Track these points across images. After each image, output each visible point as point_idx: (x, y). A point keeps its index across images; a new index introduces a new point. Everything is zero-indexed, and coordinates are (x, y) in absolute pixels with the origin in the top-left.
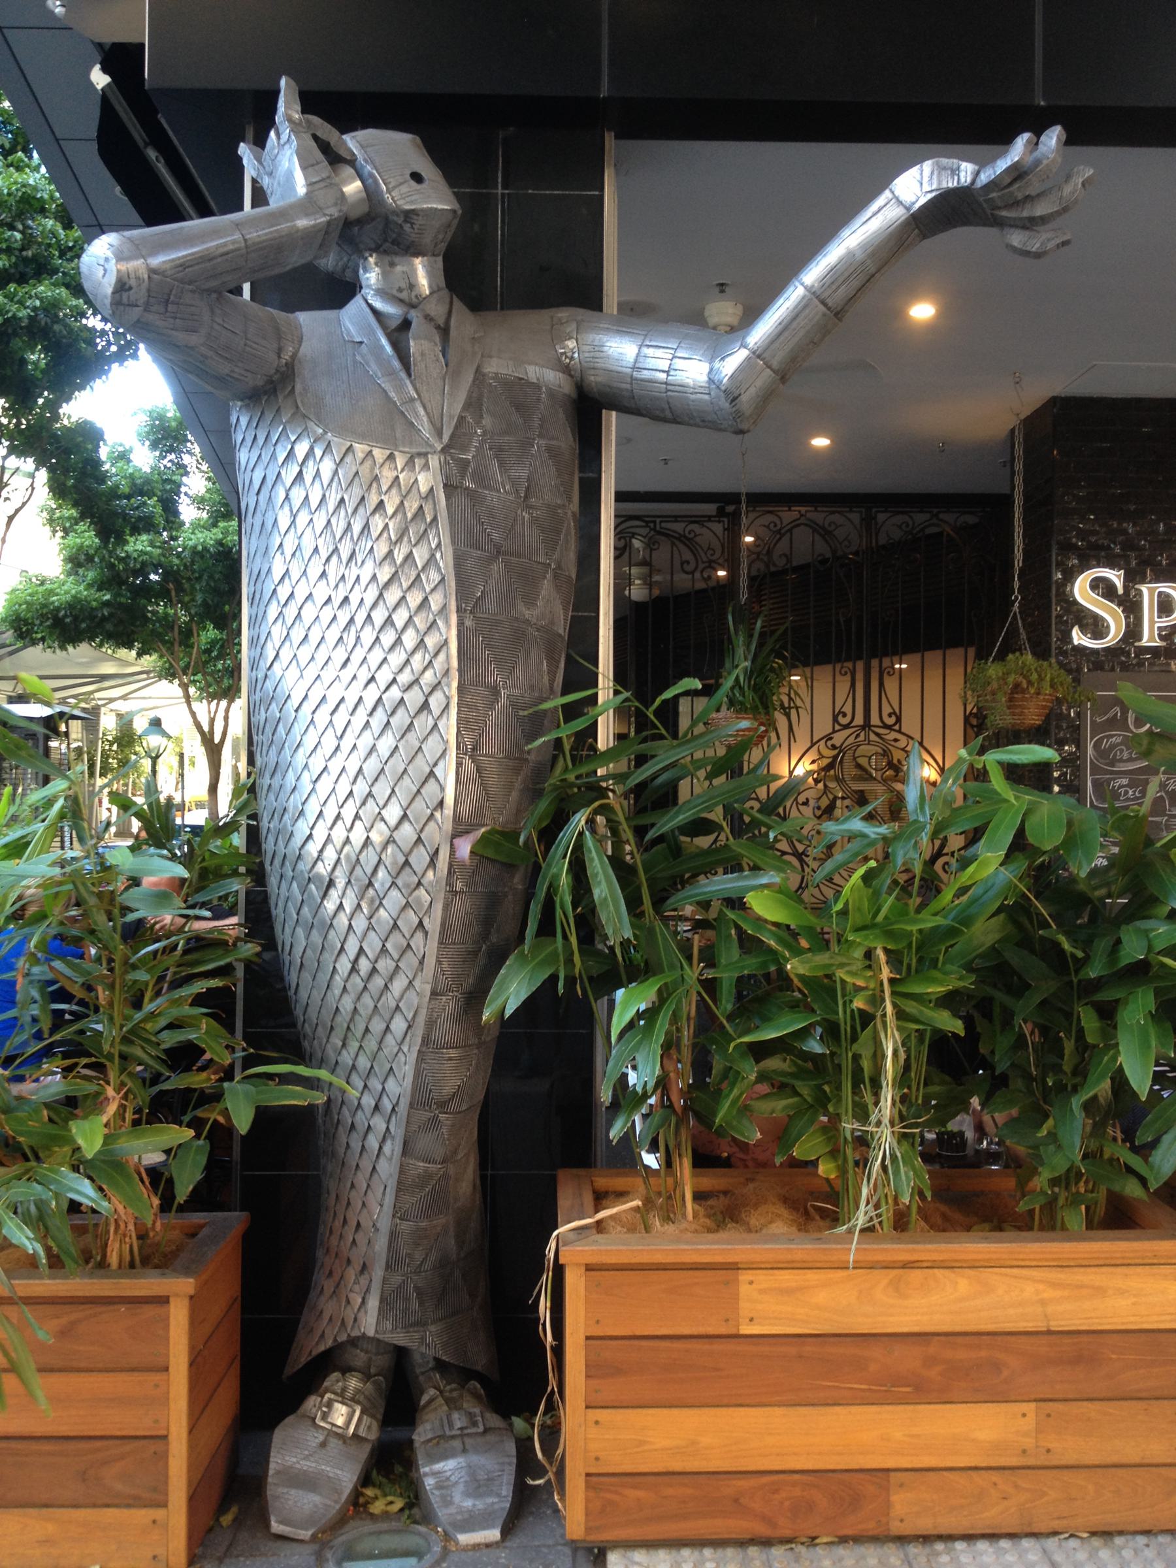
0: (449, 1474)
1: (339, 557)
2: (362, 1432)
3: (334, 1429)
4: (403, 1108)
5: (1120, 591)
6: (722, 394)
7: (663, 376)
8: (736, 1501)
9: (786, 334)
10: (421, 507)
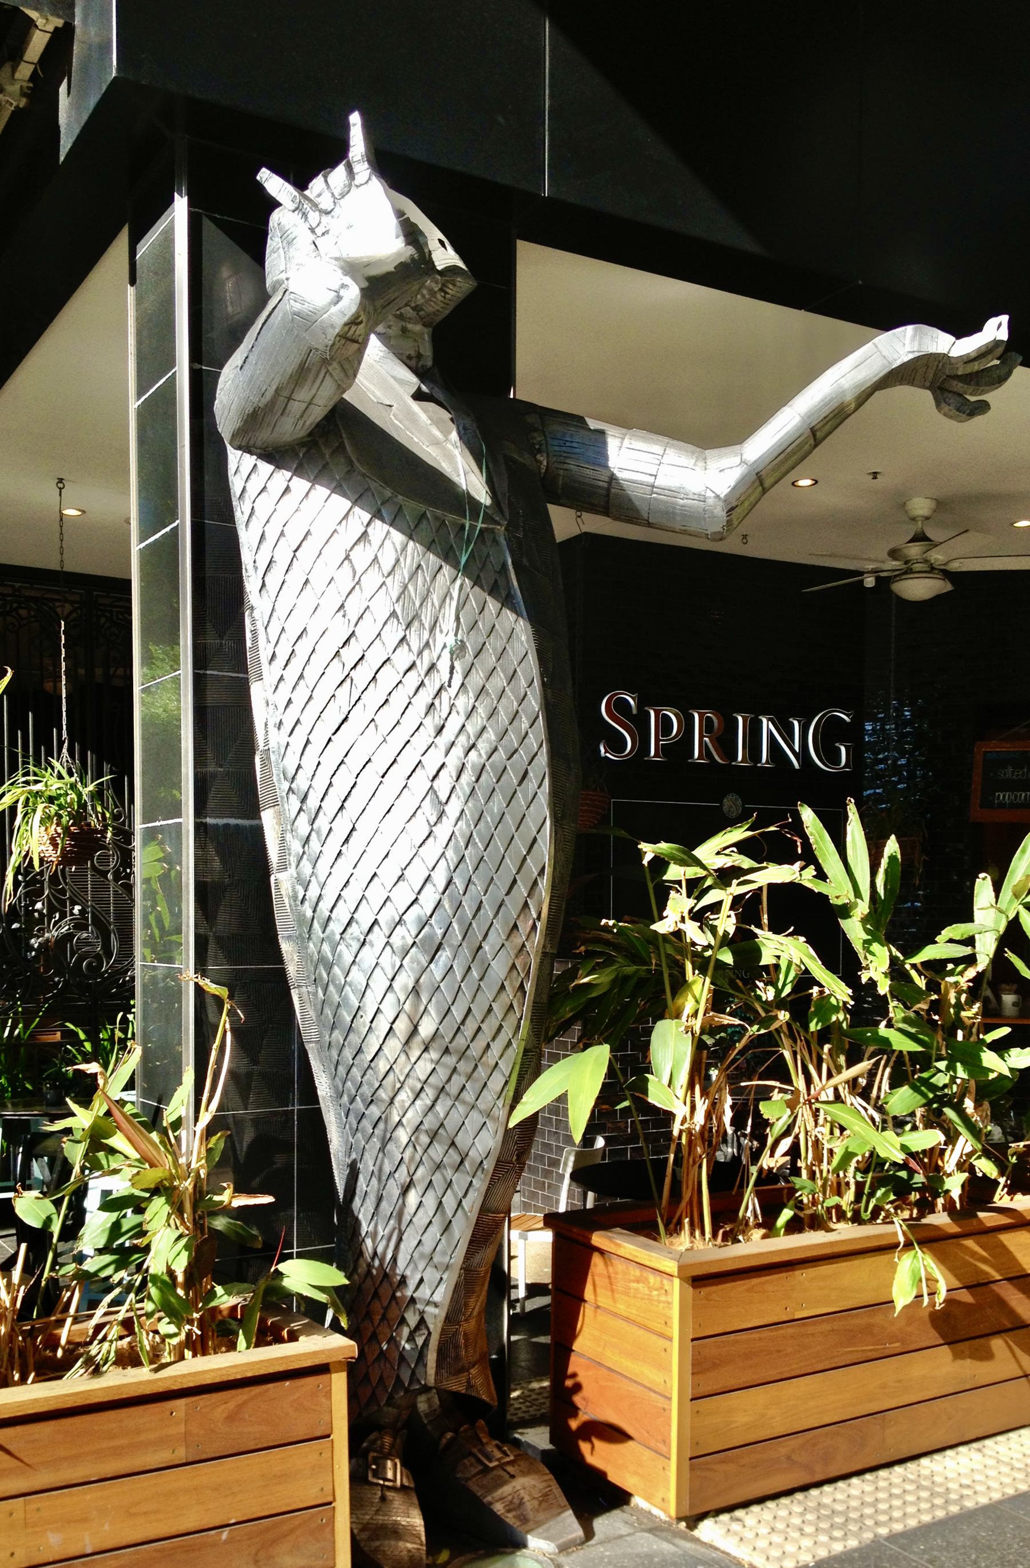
0: (510, 1498)
1: (422, 624)
2: (406, 1483)
3: (387, 1483)
4: (489, 1165)
5: (635, 711)
6: (721, 503)
7: (651, 480)
8: (789, 1458)
9: (782, 456)
10: (496, 581)
